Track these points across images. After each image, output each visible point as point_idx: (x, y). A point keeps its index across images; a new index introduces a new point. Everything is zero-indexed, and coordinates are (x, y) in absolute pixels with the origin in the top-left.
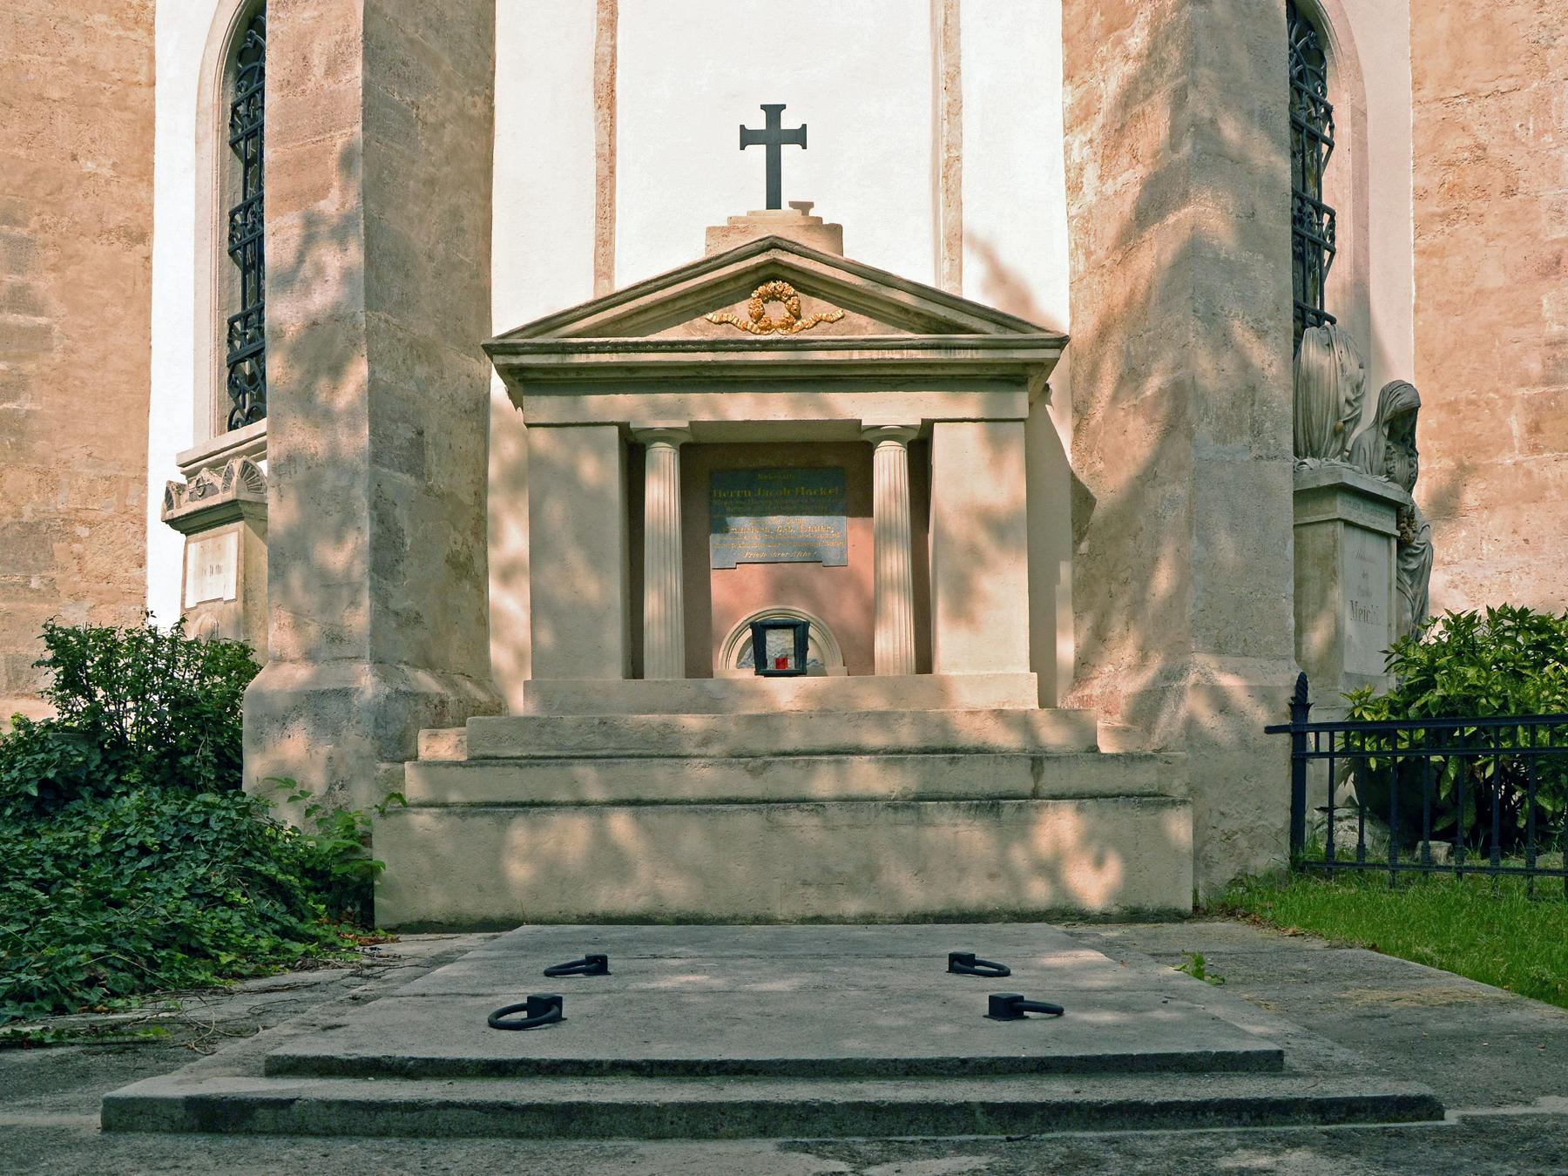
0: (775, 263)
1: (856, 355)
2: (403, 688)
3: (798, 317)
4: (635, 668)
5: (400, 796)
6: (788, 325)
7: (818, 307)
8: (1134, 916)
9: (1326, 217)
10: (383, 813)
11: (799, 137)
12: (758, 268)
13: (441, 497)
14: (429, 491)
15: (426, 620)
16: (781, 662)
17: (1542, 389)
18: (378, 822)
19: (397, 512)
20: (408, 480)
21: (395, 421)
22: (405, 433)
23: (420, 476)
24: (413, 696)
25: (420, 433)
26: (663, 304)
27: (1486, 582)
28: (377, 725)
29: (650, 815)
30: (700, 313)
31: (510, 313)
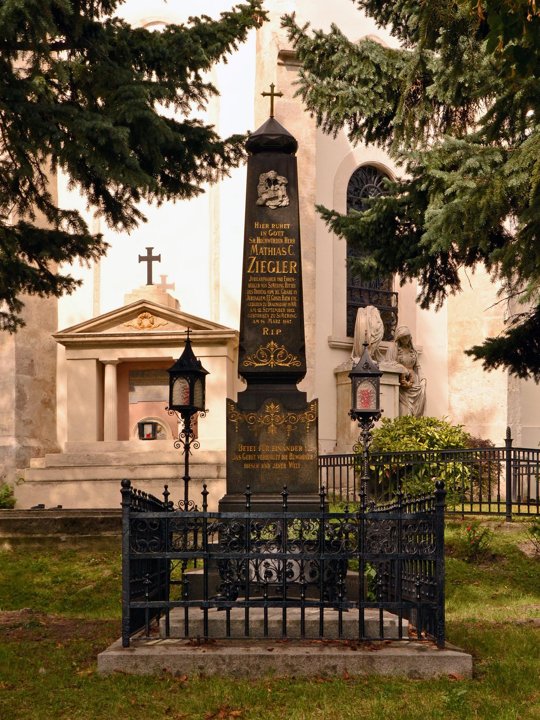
0: (144, 307)
1: (170, 337)
2: (25, 445)
3: (153, 324)
4: (101, 437)
5: (23, 479)
6: (149, 327)
7: (159, 321)
8: (48, 468)
9: (382, 259)
10: (17, 484)
11: (158, 258)
12: (139, 309)
13: (39, 381)
14: (35, 379)
15: (34, 422)
16: (148, 435)
17: (494, 317)
18: (15, 487)
19: (24, 388)
20: (28, 377)
21: (23, 359)
22: (27, 362)
23: (32, 375)
24: (29, 447)
25: (32, 361)
26: (109, 321)
27: (474, 399)
28: (17, 457)
29: (98, 484)
30: (122, 323)
31: (62, 325)
